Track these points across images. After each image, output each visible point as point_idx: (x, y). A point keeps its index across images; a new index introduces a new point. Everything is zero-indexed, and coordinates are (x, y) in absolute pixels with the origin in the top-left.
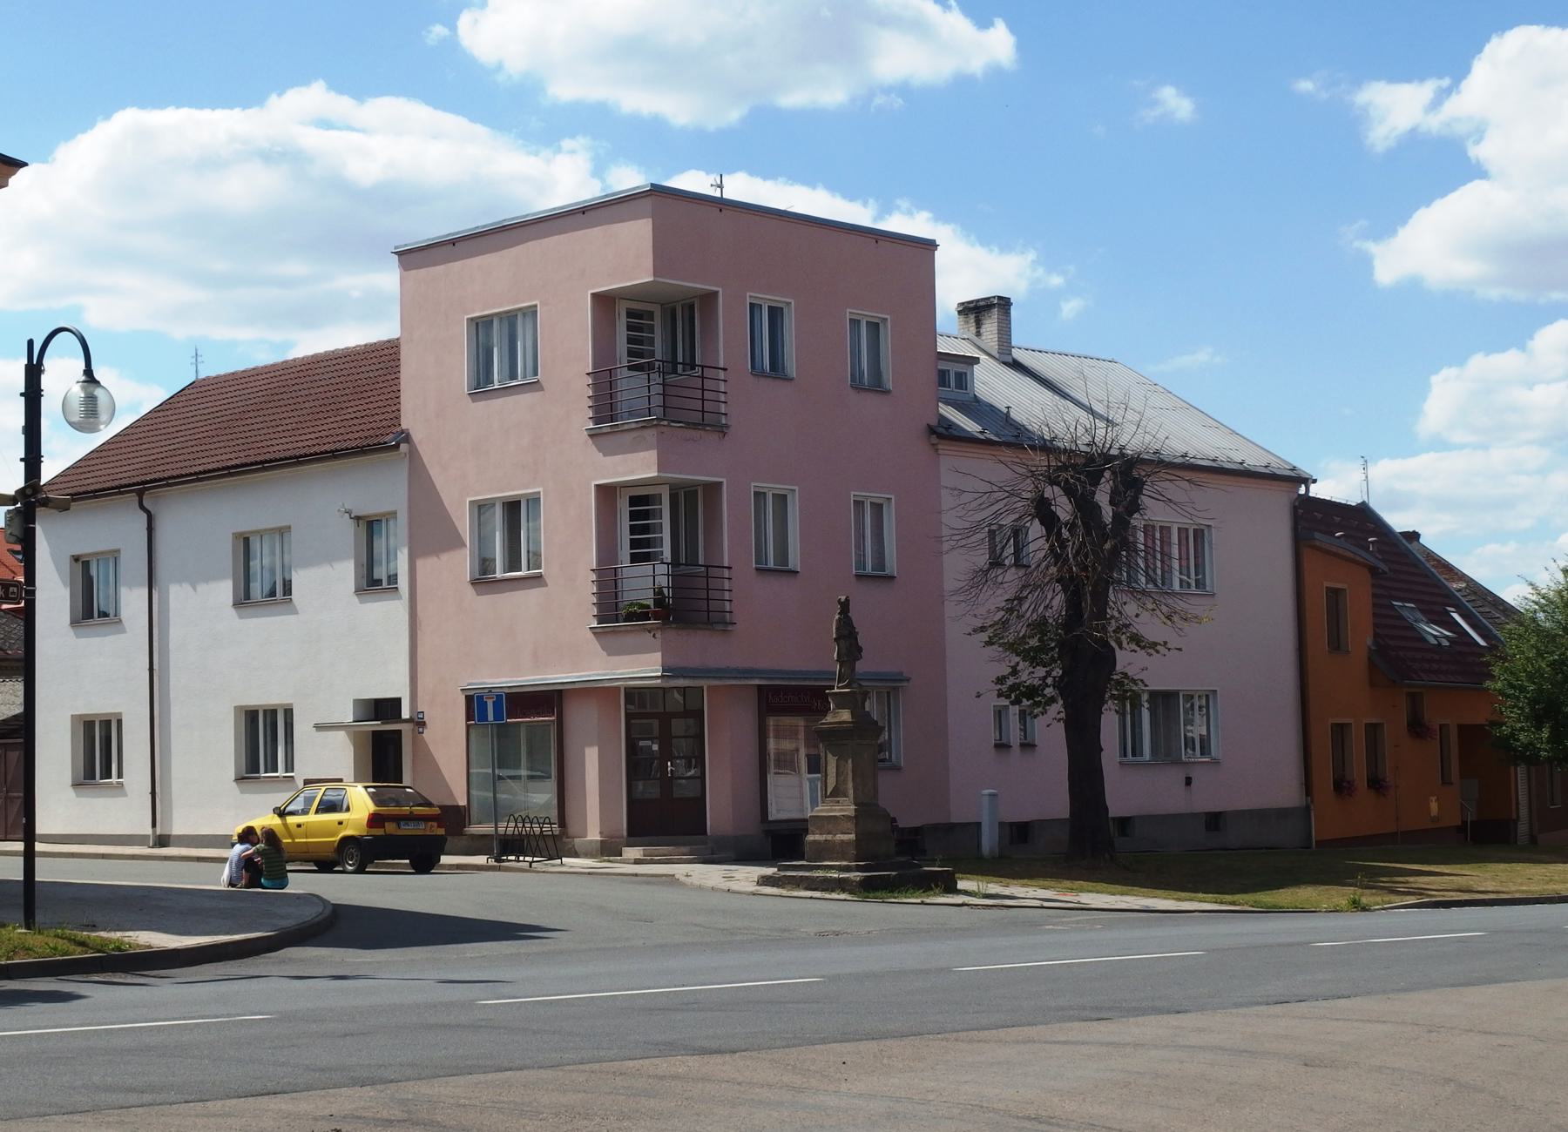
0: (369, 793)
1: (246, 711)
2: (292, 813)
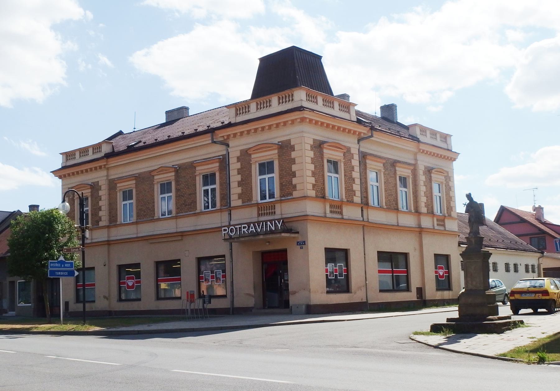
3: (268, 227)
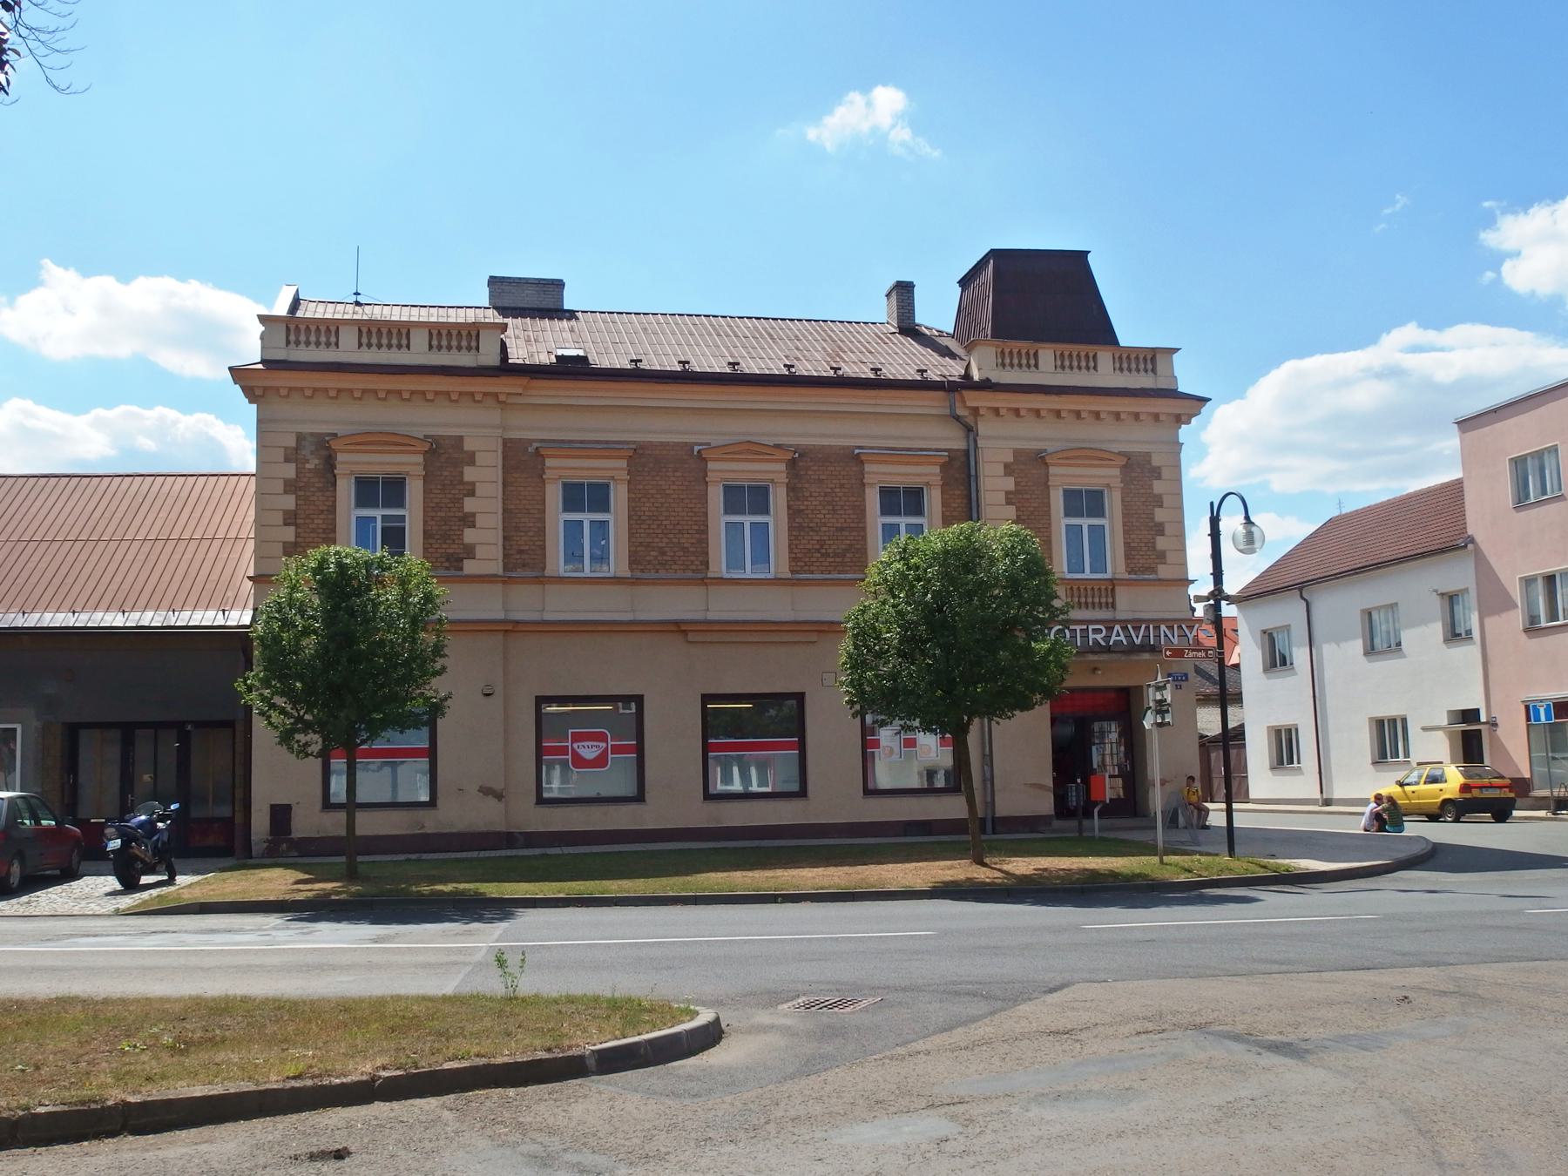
0: (1460, 771)
1: (1376, 721)
2: (1408, 784)
3: (1154, 636)
